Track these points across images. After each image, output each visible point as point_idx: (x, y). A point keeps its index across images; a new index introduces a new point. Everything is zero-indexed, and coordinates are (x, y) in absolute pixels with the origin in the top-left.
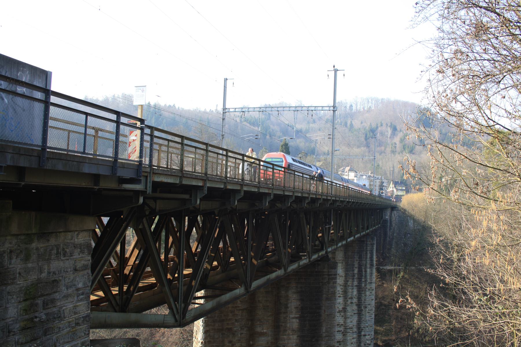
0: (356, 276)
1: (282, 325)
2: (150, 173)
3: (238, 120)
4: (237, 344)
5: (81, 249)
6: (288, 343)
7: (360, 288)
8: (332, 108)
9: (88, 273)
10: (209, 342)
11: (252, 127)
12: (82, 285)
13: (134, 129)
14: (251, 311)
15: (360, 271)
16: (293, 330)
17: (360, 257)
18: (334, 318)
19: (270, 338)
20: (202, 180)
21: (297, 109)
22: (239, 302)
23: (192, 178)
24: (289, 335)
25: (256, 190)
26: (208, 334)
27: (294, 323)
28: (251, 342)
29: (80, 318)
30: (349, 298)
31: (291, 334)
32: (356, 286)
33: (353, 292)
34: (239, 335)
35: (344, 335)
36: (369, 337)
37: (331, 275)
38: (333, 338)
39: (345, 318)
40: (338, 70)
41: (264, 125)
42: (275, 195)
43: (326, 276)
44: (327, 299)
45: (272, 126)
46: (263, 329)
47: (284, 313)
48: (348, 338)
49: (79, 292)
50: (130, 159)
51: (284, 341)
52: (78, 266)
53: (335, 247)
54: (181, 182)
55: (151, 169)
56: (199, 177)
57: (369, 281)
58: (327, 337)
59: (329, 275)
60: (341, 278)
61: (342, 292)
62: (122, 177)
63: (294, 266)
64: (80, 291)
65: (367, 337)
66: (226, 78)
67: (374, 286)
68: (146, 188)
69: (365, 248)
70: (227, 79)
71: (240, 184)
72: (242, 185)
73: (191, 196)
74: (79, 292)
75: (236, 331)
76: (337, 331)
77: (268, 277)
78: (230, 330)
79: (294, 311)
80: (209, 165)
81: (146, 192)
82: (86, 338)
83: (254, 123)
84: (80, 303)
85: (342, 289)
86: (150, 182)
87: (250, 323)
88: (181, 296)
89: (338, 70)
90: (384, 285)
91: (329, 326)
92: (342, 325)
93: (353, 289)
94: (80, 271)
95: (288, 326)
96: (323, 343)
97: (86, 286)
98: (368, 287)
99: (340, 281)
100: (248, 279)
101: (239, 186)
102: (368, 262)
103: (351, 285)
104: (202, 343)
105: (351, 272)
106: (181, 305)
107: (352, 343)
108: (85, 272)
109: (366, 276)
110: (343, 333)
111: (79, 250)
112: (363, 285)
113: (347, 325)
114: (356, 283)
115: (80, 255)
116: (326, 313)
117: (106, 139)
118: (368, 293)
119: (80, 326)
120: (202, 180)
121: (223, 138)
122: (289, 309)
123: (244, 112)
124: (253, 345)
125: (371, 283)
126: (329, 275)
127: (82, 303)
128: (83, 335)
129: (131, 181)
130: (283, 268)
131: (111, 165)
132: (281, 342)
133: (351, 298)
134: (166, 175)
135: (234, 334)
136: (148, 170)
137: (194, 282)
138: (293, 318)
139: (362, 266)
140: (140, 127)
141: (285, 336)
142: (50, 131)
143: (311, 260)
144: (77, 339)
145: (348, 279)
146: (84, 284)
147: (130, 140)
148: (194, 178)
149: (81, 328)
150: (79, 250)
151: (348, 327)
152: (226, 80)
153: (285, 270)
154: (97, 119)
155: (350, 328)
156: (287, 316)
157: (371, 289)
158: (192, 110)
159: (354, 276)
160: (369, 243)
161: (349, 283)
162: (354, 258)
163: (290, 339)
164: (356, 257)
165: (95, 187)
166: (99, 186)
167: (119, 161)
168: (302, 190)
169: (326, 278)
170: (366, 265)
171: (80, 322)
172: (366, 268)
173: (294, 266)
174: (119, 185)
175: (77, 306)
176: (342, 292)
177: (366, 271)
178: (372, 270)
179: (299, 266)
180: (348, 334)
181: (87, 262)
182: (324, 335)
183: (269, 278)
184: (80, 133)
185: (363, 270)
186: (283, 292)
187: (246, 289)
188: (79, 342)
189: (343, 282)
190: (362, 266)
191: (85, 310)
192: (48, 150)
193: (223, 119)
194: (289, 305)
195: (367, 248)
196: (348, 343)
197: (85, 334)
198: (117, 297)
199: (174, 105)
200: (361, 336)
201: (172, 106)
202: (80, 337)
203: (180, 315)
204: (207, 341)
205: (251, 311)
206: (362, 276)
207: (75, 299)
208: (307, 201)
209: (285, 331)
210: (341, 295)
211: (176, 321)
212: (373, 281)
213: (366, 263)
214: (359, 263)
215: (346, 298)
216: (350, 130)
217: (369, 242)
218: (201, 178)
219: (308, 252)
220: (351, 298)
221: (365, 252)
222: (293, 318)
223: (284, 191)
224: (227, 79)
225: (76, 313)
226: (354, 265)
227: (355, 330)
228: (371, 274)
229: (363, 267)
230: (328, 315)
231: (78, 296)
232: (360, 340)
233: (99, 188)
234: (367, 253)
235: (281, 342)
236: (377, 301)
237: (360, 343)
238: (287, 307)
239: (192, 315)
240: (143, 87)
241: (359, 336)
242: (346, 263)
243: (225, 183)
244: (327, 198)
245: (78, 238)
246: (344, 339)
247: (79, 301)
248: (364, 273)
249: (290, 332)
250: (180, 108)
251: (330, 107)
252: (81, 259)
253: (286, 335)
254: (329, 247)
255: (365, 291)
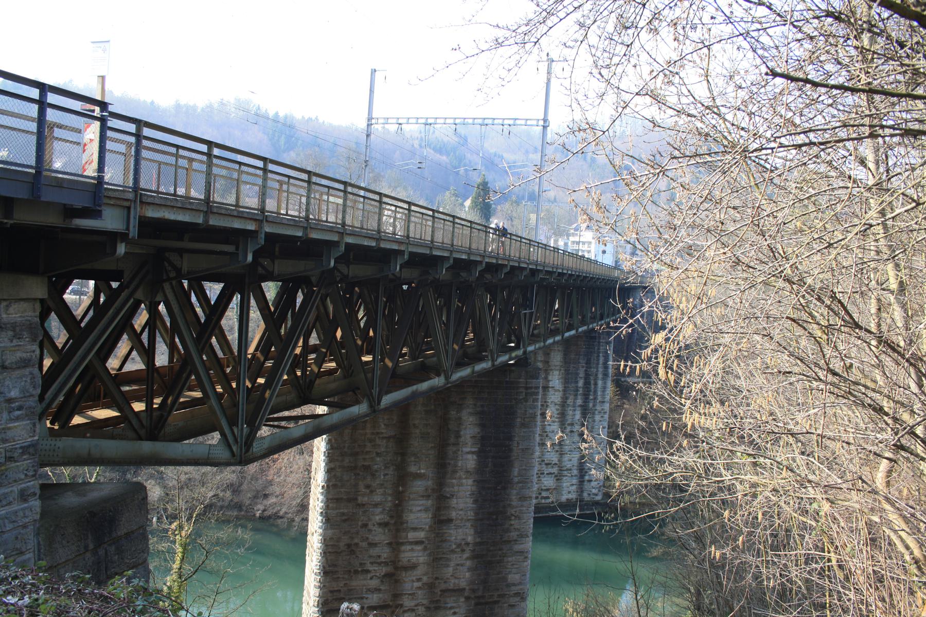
0: (581, 391)
1: (449, 464)
2: (135, 201)
3: (416, 146)
4: (378, 491)
5: (14, 331)
6: (458, 491)
7: (586, 410)
8: (541, 123)
9: (31, 373)
10: (335, 486)
11: (438, 155)
12: (18, 393)
13: (90, 121)
14: (401, 440)
15: (587, 383)
16: (467, 472)
17: (588, 362)
18: (532, 454)
19: (430, 483)
20: (255, 220)
21: (486, 122)
22: (383, 426)
23: (230, 215)
24: (460, 478)
25: (374, 244)
26: (333, 474)
27: (469, 461)
28: (401, 488)
29: (16, 449)
30: (569, 424)
31: (464, 477)
32: (580, 406)
33: (574, 415)
34: (382, 477)
35: (557, 480)
36: (596, 483)
37: (531, 388)
38: (529, 485)
39: (560, 454)
40: (553, 61)
41: (457, 154)
42: (411, 254)
43: (524, 390)
44: (523, 425)
45: (468, 156)
46: (420, 469)
47: (454, 444)
48: (565, 484)
49: (13, 405)
50: (85, 174)
51: (453, 487)
52: (9, 361)
53: (542, 344)
54: (206, 220)
55: (136, 196)
56: (245, 215)
57: (599, 398)
58: (520, 483)
59: (527, 388)
60: (556, 393)
61: (558, 414)
62: (72, 205)
63: (465, 372)
64: (15, 402)
65: (593, 484)
66: (373, 68)
67: (607, 407)
68: (128, 229)
69: (596, 348)
70: (375, 71)
71: (339, 233)
72: (342, 233)
73: (237, 249)
74: (13, 405)
75: (376, 471)
76: (547, 474)
77: (414, 388)
78: (367, 468)
79: (469, 441)
80: (412, 226)
81: (128, 234)
82: (30, 482)
83: (441, 149)
84: (16, 424)
85: (557, 410)
86: (135, 218)
87: (399, 459)
88: (243, 415)
89: (553, 61)
90: (625, 406)
91: (524, 467)
92: (556, 464)
93: (575, 410)
94: (13, 369)
95: (460, 465)
96: (514, 492)
97: (28, 394)
98: (598, 408)
99: (555, 397)
100: (375, 392)
101: (337, 235)
102: (601, 370)
103: (571, 404)
104: (323, 487)
105: (573, 385)
106: (242, 429)
107: (569, 492)
108: (27, 371)
109: (595, 392)
110: (556, 476)
111: (10, 333)
112: (591, 405)
113: (564, 464)
114: (579, 401)
115: (14, 341)
116: (520, 447)
117: (14, 129)
118: (597, 418)
119: (16, 461)
120: (255, 220)
121: (366, 166)
122: (462, 439)
123: (400, 124)
124: (403, 492)
125: (603, 402)
126: (527, 388)
127: (21, 423)
128: (23, 477)
129: (86, 213)
130: (442, 375)
131: (30, 179)
132: (448, 490)
133: (572, 424)
134: (173, 207)
135: (373, 475)
136: (131, 196)
137: (268, 392)
138: (468, 453)
139: (590, 375)
140: (99, 116)
141: (454, 481)
142: (143, 164)
143: (496, 363)
144: (10, 484)
145: (567, 395)
146: (23, 390)
147: (85, 141)
148: (235, 216)
149: (17, 466)
150: (10, 333)
151: (565, 468)
152: (374, 71)
153: (447, 378)
154: (10, 98)
155: (567, 470)
156: (459, 450)
157: (602, 412)
158: (344, 125)
159: (577, 391)
160: (604, 341)
161: (570, 402)
162: (579, 363)
163: (462, 485)
164: (583, 362)
165: (6, 221)
166: (12, 218)
167: (45, 173)
168: (520, 258)
169: (522, 392)
170: (596, 375)
171: (16, 455)
172: (596, 379)
173: (465, 372)
174: (64, 221)
175: (9, 429)
176: (558, 414)
177: (596, 384)
178: (605, 383)
179: (473, 372)
180: (565, 478)
181: (28, 354)
182: (516, 480)
183: (417, 390)
184: (171, 165)
185: (592, 382)
186: (452, 413)
187: (371, 406)
188: (15, 489)
189: (559, 399)
190: (590, 375)
191: (25, 435)
192: (105, 186)
193: (368, 136)
194: (462, 433)
195: (599, 349)
196: (564, 493)
197: (26, 475)
198: (143, 415)
199: (316, 118)
200: (583, 481)
201: (313, 119)
202: (15, 481)
203: (241, 445)
204: (331, 484)
205: (401, 440)
206: (590, 391)
207: (4, 416)
208: (447, 265)
209: (455, 472)
210: (557, 420)
211: (233, 455)
212: (606, 400)
213: (597, 371)
214: (586, 371)
215: (564, 424)
216: (591, 166)
217: (603, 339)
218: (250, 216)
219: (491, 350)
220: (572, 424)
221: (596, 355)
222: (468, 453)
223: (431, 248)
224: (375, 71)
225: (7, 440)
226: (577, 374)
227: (575, 472)
228: (604, 388)
229: (592, 378)
230: (523, 450)
231: (10, 412)
232: (582, 488)
233: (15, 223)
234: (598, 356)
235: (448, 489)
236: (611, 430)
237: (582, 492)
238: (458, 436)
239: (265, 446)
240: (106, 44)
241: (580, 481)
242: (565, 370)
243: (305, 228)
244: (469, 257)
245: (8, 312)
246: (557, 486)
247: (11, 420)
248: (593, 386)
249: (461, 474)
250: (326, 123)
251: (538, 120)
252: (17, 348)
253: (455, 479)
254: (530, 344)
255: (594, 414)
